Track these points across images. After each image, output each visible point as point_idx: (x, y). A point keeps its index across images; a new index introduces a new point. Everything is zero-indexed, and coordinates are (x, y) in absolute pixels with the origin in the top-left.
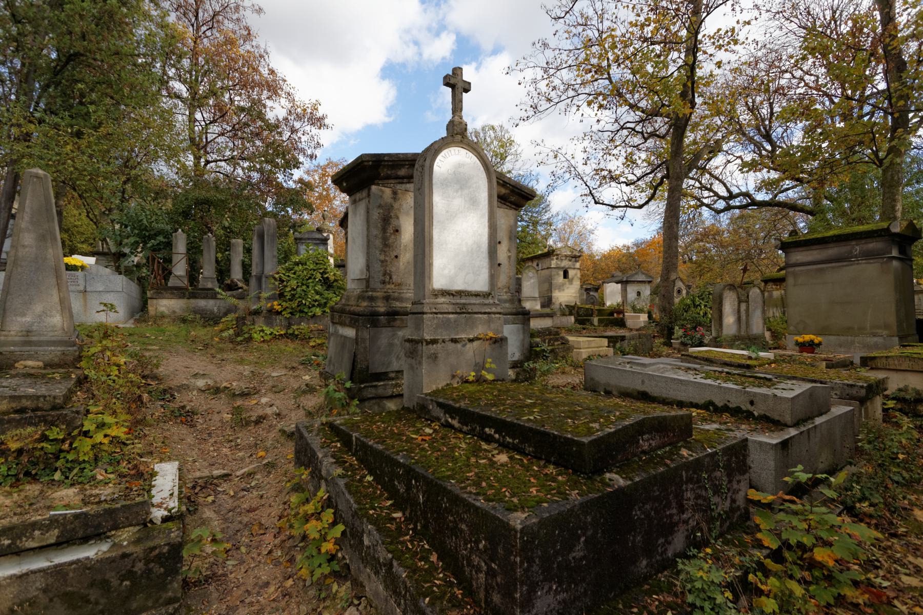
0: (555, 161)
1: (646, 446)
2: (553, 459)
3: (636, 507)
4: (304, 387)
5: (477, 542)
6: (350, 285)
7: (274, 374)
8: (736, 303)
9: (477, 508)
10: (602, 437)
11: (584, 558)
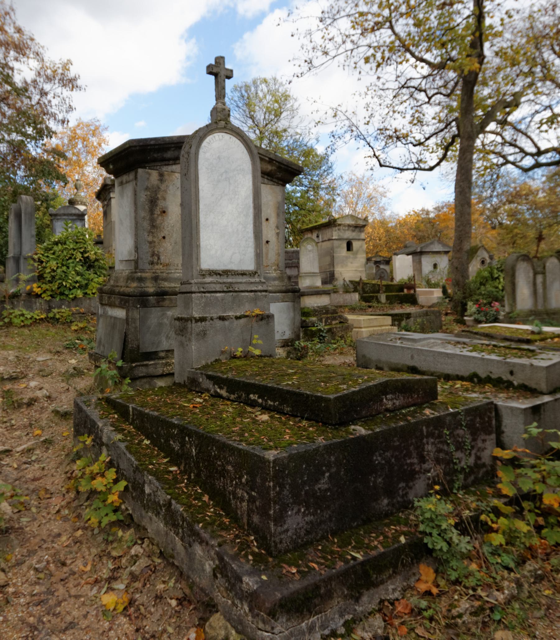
0: (334, 120)
1: (390, 405)
2: (306, 416)
3: (377, 454)
4: (71, 371)
5: (240, 478)
6: (118, 267)
7: (40, 359)
8: (531, 275)
9: (240, 450)
10: (347, 395)
11: (326, 490)
